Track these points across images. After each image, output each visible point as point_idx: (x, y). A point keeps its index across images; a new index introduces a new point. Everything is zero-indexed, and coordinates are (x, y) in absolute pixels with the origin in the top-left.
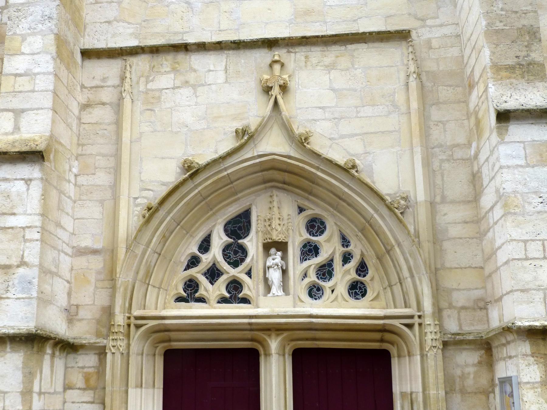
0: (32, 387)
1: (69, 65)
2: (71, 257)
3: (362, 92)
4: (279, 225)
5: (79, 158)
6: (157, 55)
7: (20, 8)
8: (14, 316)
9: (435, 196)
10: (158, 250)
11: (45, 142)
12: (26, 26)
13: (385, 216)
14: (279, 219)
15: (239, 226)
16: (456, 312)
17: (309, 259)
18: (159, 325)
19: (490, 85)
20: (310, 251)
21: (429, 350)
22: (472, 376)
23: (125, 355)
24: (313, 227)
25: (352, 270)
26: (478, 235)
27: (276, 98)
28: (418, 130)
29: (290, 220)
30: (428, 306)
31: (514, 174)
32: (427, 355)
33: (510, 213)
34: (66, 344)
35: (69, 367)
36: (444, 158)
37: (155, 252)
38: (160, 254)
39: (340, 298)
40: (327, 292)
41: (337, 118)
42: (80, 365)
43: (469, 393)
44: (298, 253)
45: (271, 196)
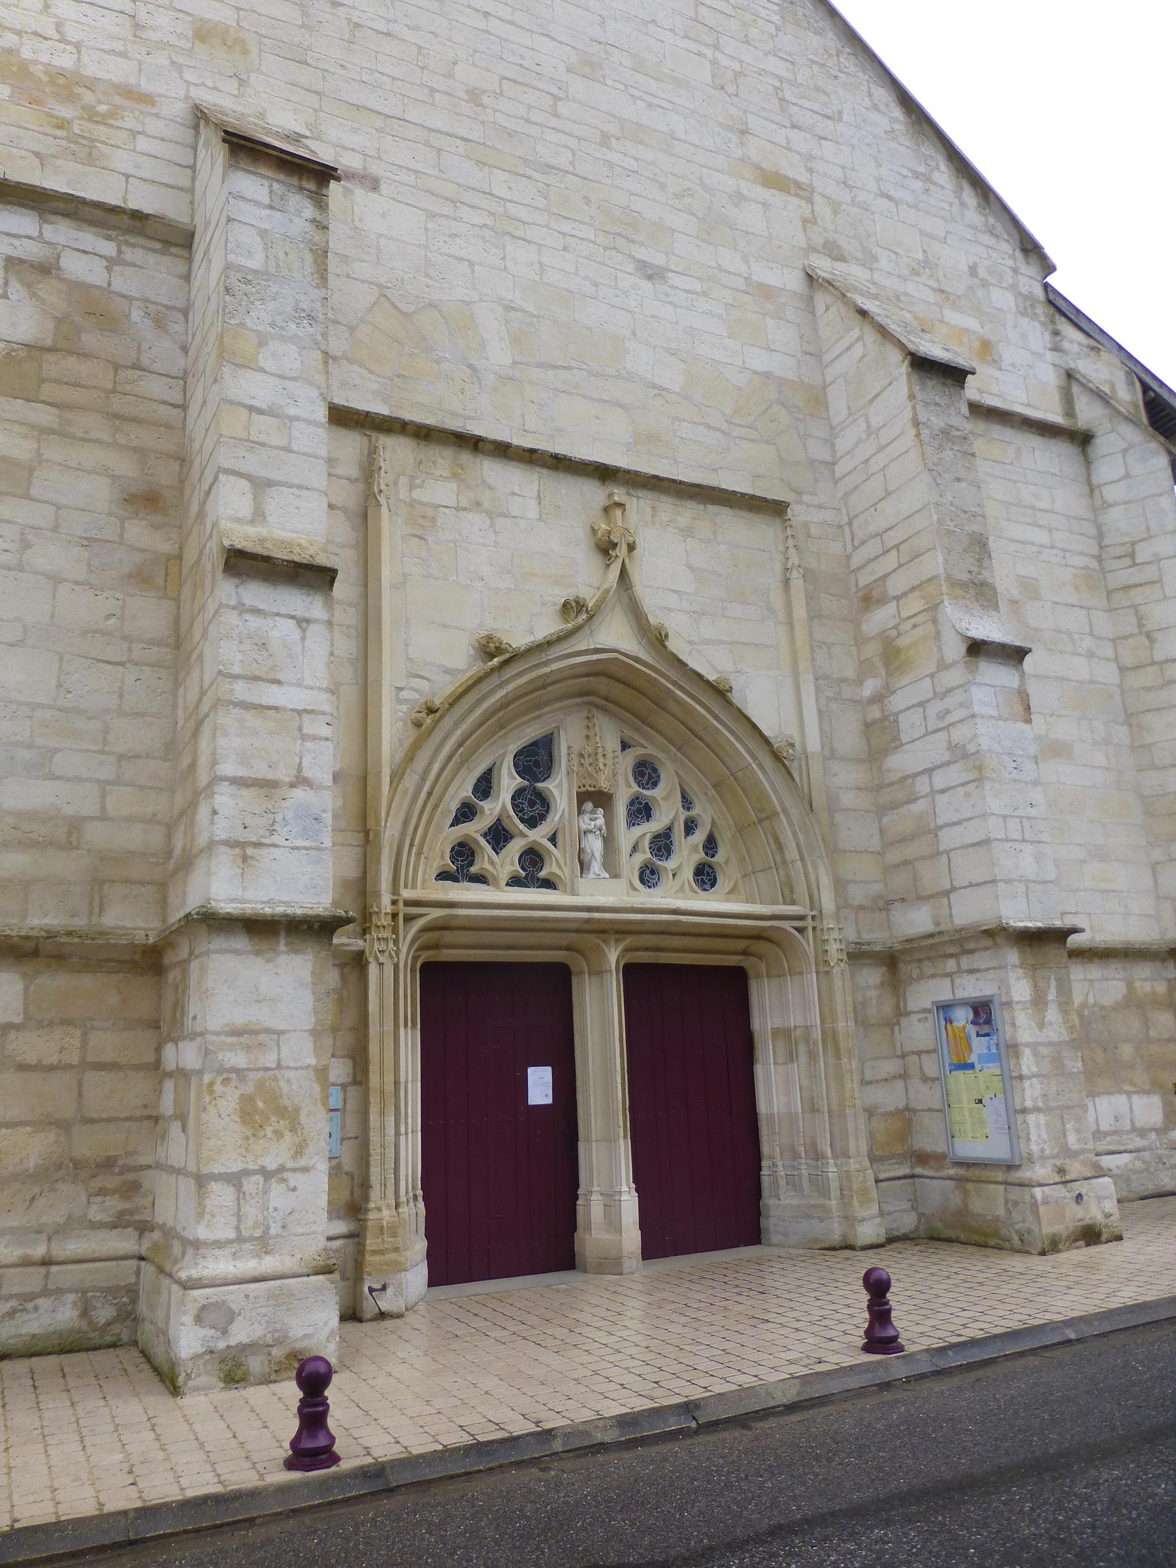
7: (250, 277)
15: (536, 760)
22: (874, 1002)
24: (642, 774)
39: (687, 888)
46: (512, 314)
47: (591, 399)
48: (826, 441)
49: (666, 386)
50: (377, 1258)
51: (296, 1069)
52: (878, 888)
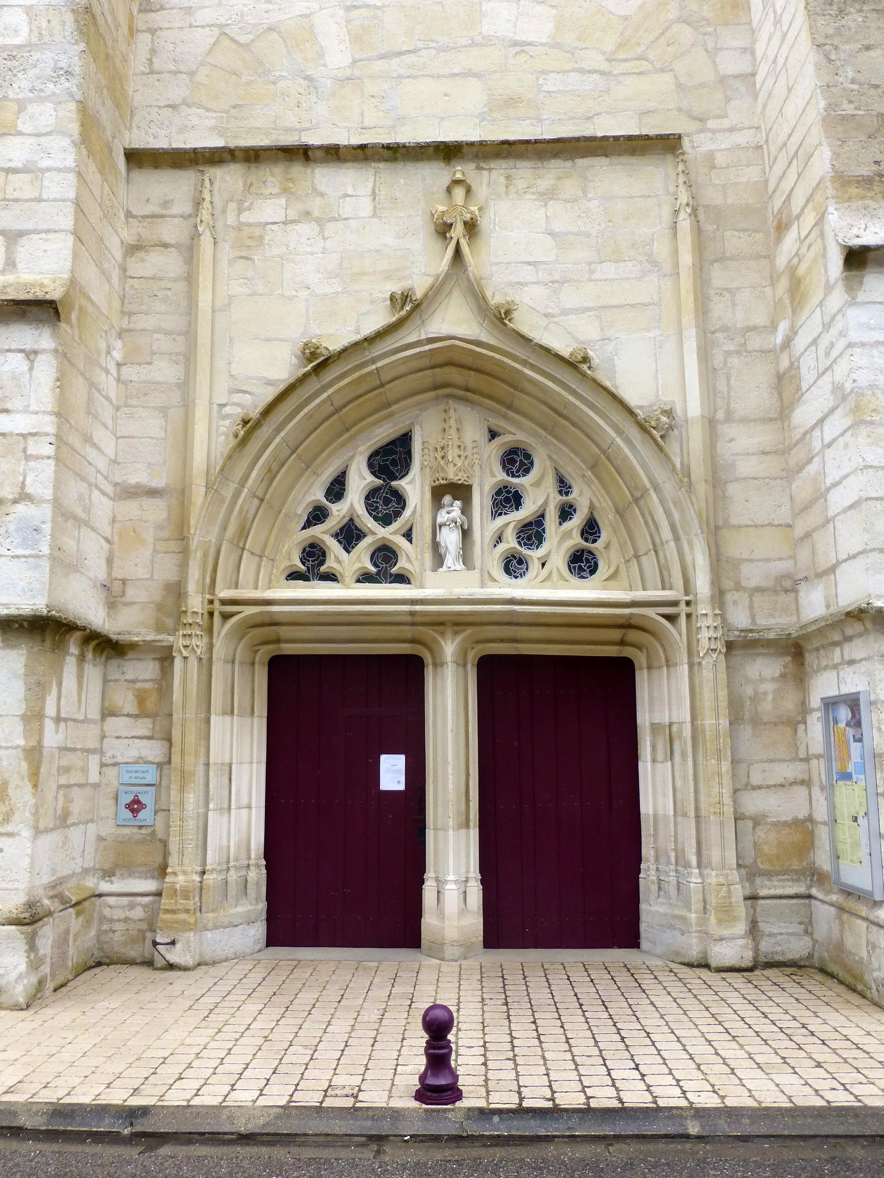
0: (43, 708)
1: (105, 168)
2: (113, 499)
3: (599, 240)
4: (459, 456)
5: (124, 335)
6: (256, 165)
7: (14, 53)
8: (9, 586)
9: (715, 410)
10: (260, 493)
11: (62, 289)
12: (25, 84)
13: (635, 443)
14: (459, 447)
15: (392, 459)
16: (746, 595)
17: (506, 514)
18: (261, 613)
19: (831, 209)
20: (507, 500)
21: (705, 654)
22: (770, 697)
23: (204, 661)
24: (512, 462)
25: (575, 531)
26: (784, 474)
27: (458, 242)
28: (692, 299)
29: (475, 450)
30: (702, 585)
31: (872, 356)
32: (700, 664)
33: (863, 422)
34: (104, 642)
35: (111, 681)
36: (732, 348)
37: (254, 496)
38: (262, 500)
40: (535, 566)
41: (556, 282)
42: (129, 676)
43: (766, 723)
44: (489, 503)
45: (446, 411)
46: (355, 13)
47: (439, 76)
48: (745, 50)
49: (530, 40)
50: (169, 916)
51: (7, 748)
52: (783, 566)
